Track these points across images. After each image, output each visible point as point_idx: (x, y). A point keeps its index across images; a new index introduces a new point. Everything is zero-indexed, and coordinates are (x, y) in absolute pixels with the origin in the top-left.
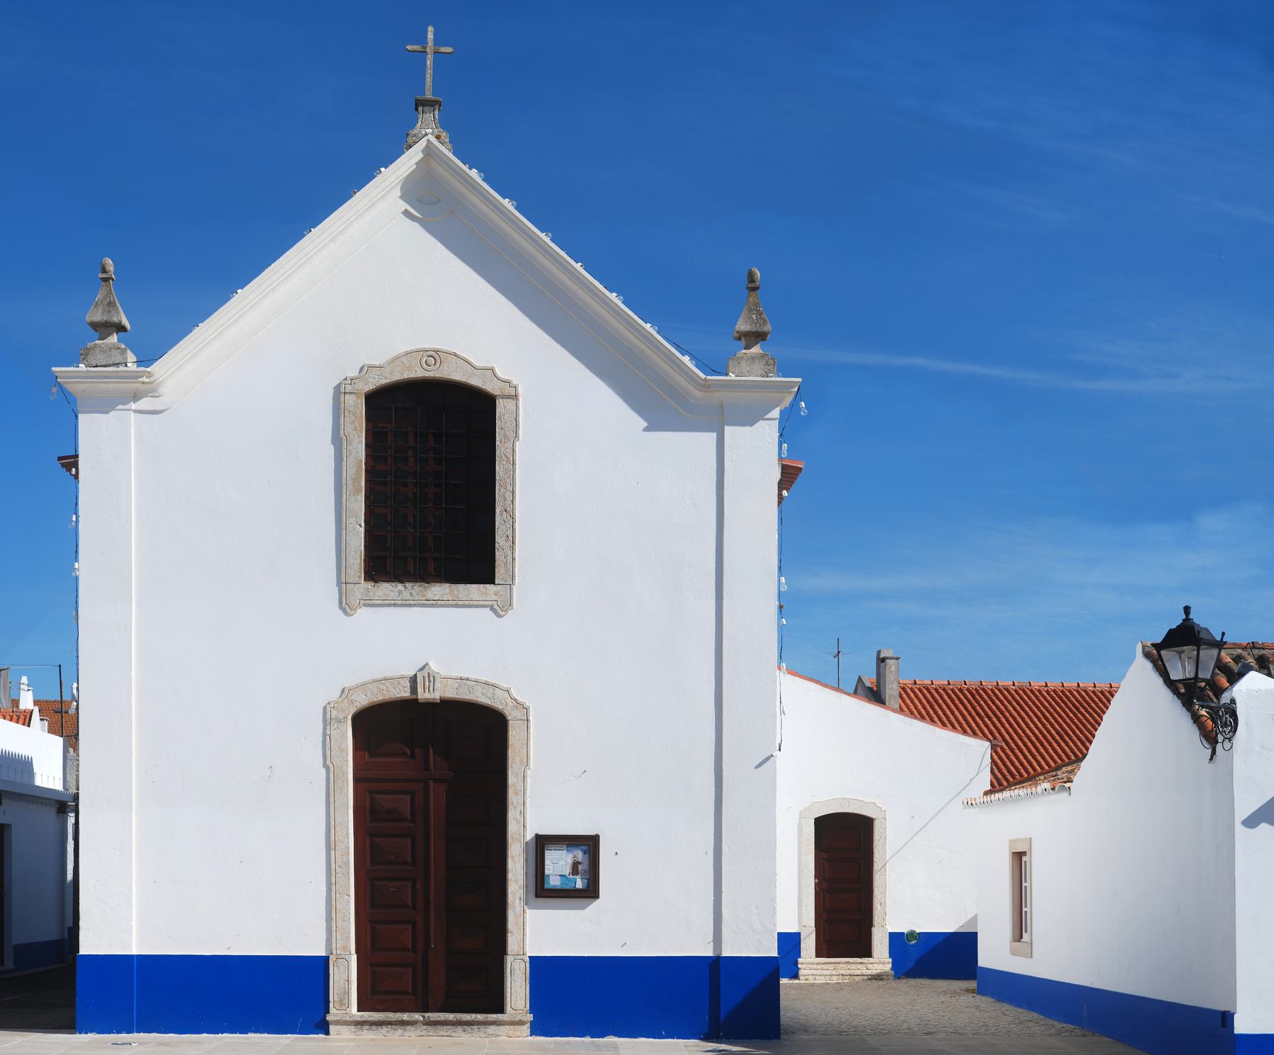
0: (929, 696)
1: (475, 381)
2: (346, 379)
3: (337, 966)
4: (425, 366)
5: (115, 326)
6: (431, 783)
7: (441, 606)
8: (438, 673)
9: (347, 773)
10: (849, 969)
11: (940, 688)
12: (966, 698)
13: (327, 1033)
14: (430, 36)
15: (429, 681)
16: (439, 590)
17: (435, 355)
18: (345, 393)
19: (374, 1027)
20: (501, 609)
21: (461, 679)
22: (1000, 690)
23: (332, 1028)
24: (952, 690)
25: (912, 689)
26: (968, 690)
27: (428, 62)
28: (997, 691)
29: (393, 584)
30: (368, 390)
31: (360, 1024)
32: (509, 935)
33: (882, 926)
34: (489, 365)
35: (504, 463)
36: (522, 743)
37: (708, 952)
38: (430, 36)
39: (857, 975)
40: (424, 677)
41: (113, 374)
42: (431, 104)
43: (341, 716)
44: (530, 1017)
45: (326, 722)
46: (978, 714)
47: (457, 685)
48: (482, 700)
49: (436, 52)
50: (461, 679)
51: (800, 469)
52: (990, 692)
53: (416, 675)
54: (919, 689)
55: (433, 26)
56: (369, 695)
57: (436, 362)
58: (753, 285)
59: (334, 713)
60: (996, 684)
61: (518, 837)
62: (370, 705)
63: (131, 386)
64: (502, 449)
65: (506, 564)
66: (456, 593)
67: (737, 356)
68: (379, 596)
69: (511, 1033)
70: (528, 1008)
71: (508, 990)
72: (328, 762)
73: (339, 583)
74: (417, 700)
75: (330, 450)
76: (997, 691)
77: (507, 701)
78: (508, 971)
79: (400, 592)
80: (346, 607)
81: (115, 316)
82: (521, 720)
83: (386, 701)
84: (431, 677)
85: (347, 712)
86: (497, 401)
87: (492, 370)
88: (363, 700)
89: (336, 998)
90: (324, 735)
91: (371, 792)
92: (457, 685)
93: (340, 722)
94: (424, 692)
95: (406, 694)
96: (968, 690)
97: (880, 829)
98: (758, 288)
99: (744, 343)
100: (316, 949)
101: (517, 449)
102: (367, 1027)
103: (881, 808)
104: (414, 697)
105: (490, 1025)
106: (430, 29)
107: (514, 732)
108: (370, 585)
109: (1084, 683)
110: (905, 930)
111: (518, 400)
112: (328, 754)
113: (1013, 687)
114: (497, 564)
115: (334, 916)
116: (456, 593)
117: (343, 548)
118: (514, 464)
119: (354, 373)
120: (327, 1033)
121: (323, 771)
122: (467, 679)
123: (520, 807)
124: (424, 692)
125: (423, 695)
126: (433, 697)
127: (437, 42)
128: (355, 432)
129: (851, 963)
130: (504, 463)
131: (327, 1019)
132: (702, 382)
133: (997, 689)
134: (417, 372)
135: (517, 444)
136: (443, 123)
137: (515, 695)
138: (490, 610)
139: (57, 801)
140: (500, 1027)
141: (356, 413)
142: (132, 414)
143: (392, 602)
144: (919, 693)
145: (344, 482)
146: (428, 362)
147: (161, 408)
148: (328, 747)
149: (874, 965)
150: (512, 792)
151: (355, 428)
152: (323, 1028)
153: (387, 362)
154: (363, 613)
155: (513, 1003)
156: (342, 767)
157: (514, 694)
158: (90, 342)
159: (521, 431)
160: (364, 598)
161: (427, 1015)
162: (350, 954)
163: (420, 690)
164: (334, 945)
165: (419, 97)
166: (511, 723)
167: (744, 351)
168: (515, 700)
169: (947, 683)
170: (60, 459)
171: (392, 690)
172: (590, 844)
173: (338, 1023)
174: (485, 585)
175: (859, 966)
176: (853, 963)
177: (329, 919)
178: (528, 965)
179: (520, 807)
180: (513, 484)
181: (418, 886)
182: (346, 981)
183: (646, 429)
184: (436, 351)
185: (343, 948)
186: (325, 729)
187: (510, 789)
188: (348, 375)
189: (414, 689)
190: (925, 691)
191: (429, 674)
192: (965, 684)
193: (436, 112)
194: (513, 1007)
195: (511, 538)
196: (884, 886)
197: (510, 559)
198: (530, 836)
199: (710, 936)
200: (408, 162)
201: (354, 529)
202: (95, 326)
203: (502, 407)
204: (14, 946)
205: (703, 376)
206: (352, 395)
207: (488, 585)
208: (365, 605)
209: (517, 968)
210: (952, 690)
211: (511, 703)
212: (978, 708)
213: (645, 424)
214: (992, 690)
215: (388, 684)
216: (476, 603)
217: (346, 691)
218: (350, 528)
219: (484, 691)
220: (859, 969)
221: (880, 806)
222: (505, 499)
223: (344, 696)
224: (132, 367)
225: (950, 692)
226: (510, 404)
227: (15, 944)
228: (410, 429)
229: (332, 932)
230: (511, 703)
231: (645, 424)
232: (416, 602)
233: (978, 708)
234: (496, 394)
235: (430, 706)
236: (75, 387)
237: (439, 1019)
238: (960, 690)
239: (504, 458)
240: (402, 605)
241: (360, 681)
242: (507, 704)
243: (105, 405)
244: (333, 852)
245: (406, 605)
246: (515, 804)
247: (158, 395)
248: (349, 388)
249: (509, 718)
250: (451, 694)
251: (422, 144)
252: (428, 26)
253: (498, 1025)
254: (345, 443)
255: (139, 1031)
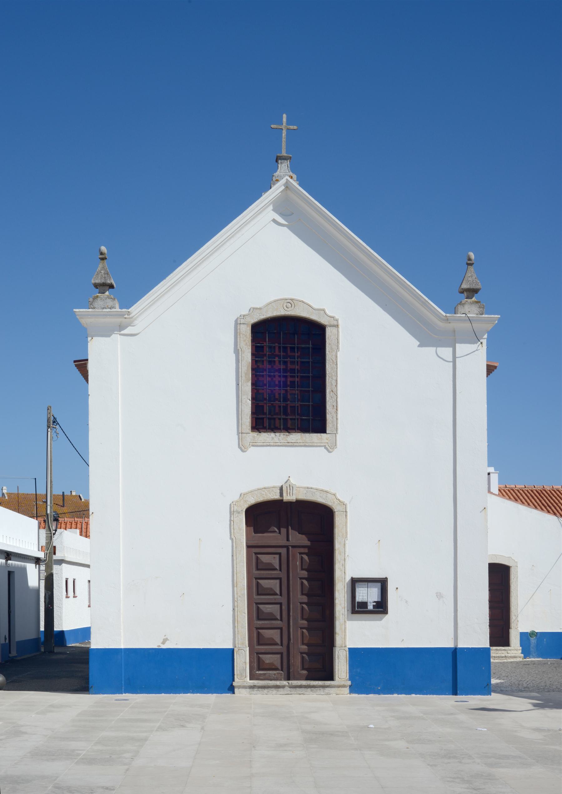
0: (514, 494)
1: (314, 317)
2: (241, 316)
3: (238, 654)
4: (285, 308)
5: (108, 286)
6: (290, 547)
7: (296, 446)
8: (295, 485)
9: (243, 543)
10: (497, 653)
11: (520, 489)
12: (535, 495)
13: (234, 693)
14: (284, 120)
15: (290, 489)
16: (296, 437)
17: (291, 302)
18: (240, 324)
19: (260, 689)
20: (330, 448)
21: (308, 488)
22: (554, 491)
23: (236, 690)
24: (527, 491)
25: (504, 490)
26: (536, 490)
27: (283, 135)
28: (553, 492)
29: (269, 434)
30: (253, 322)
31: (252, 687)
32: (337, 635)
33: (516, 628)
34: (322, 308)
35: (331, 364)
36: (343, 525)
37: (451, 645)
38: (284, 120)
39: (503, 657)
40: (287, 487)
41: (109, 313)
42: (285, 158)
43: (240, 510)
44: (349, 683)
45: (232, 513)
46: (543, 505)
47: (305, 492)
48: (320, 500)
49: (288, 129)
50: (308, 488)
51: (496, 367)
52: (549, 492)
53: (282, 486)
54: (509, 490)
55: (286, 114)
56: (255, 497)
57: (286, 306)
58: (469, 262)
59: (236, 508)
60: (543, 487)
61: (341, 579)
62: (256, 503)
63: (118, 320)
64: (330, 356)
65: (333, 422)
66: (304, 438)
67: (462, 303)
68: (261, 441)
69: (338, 692)
70: (348, 677)
71: (337, 667)
72: (233, 537)
73: (238, 433)
74: (282, 500)
75: (234, 356)
76: (553, 492)
77: (335, 501)
78: (337, 656)
79: (273, 438)
80: (242, 448)
81: (109, 280)
82: (342, 511)
83: (264, 501)
84: (291, 487)
85: (243, 507)
86: (327, 328)
87: (324, 310)
88: (252, 500)
89: (238, 672)
90: (230, 520)
91: (256, 554)
92: (305, 492)
93: (239, 513)
94: (287, 495)
95: (277, 496)
96: (536, 490)
97: (514, 572)
98: (473, 264)
99: (466, 295)
100: (228, 645)
101: (338, 355)
102: (256, 689)
103: (514, 560)
104: (281, 498)
105: (326, 687)
106: (285, 116)
107: (338, 519)
108: (255, 434)
109: (509, 485)
110: (528, 631)
111: (339, 328)
112: (232, 531)
113: (534, 488)
114: (328, 422)
115: (236, 625)
116: (304, 438)
117: (240, 413)
118: (336, 364)
119: (246, 312)
120: (234, 693)
121: (230, 541)
122: (311, 488)
123: (342, 562)
124: (287, 495)
125: (287, 498)
126: (292, 499)
127: (288, 123)
128: (246, 346)
129: (498, 650)
130: (331, 364)
131: (233, 684)
132: (444, 318)
133: (552, 490)
134: (281, 312)
135: (338, 353)
136: (293, 169)
137: (339, 497)
138: (325, 448)
139: (35, 558)
140: (332, 689)
141: (247, 335)
142: (119, 336)
143: (268, 444)
144: (508, 493)
145: (240, 375)
146: (288, 306)
147: (138, 332)
148: (232, 527)
149: (512, 651)
150: (338, 553)
151: (246, 344)
152: (231, 689)
153: (264, 305)
154: (252, 450)
155: (339, 675)
156: (240, 539)
157: (338, 496)
158: (95, 294)
159: (340, 346)
160: (252, 442)
161: (290, 682)
162: (246, 647)
163: (285, 494)
164: (237, 642)
165: (279, 155)
166: (336, 513)
167: (466, 300)
168: (339, 500)
169: (524, 487)
170: (75, 361)
171: (269, 494)
172: (383, 583)
173: (239, 687)
174: (321, 434)
175: (503, 652)
176: (500, 650)
177: (234, 627)
178: (348, 653)
179: (342, 562)
180: (337, 376)
181: (283, 607)
182: (244, 662)
183: (419, 346)
184: (292, 300)
185: (242, 643)
186: (231, 517)
187: (336, 551)
188: (242, 313)
189: (281, 494)
190: (512, 491)
191: (290, 485)
192: (535, 487)
193: (288, 162)
194: (339, 677)
195: (335, 407)
196: (517, 605)
197: (335, 419)
198: (348, 579)
199: (452, 636)
200: (276, 190)
201: (246, 402)
202: (96, 286)
203: (329, 332)
204: (16, 642)
205: (444, 314)
206: (244, 325)
207: (323, 434)
208: (253, 446)
209: (341, 654)
210: (527, 491)
211: (336, 502)
212: (543, 501)
213: (418, 343)
214: (550, 491)
215: (266, 491)
216: (316, 444)
217: (242, 495)
218: (244, 401)
219: (321, 495)
220: (503, 654)
221: (514, 559)
222: (332, 384)
223: (241, 498)
224: (118, 309)
225: (526, 492)
226: (334, 330)
227: (2, 643)
228: (277, 344)
229: (235, 634)
230: (336, 502)
231: (418, 343)
232: (281, 444)
233: (543, 501)
234: (326, 324)
235: (290, 504)
236: (84, 321)
237: (297, 684)
238: (532, 491)
239: (331, 361)
240: (273, 446)
241: (250, 490)
242: (334, 503)
243: (106, 332)
244: (235, 588)
245: (276, 446)
246: (339, 560)
247: (136, 324)
248: (242, 321)
249: (335, 510)
250: (302, 496)
251: (283, 181)
252: (283, 114)
253: (331, 688)
254: (240, 352)
255: (125, 693)
